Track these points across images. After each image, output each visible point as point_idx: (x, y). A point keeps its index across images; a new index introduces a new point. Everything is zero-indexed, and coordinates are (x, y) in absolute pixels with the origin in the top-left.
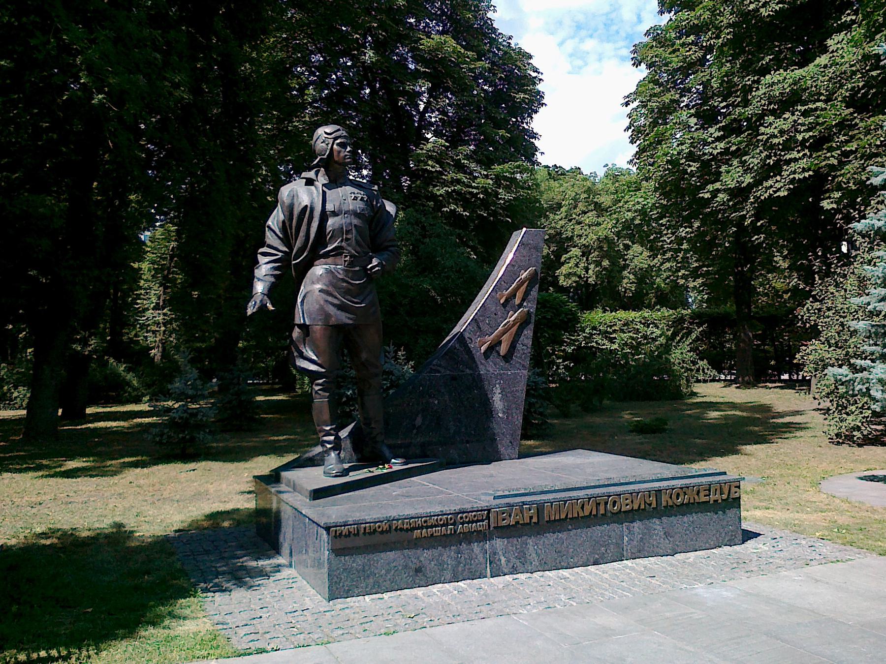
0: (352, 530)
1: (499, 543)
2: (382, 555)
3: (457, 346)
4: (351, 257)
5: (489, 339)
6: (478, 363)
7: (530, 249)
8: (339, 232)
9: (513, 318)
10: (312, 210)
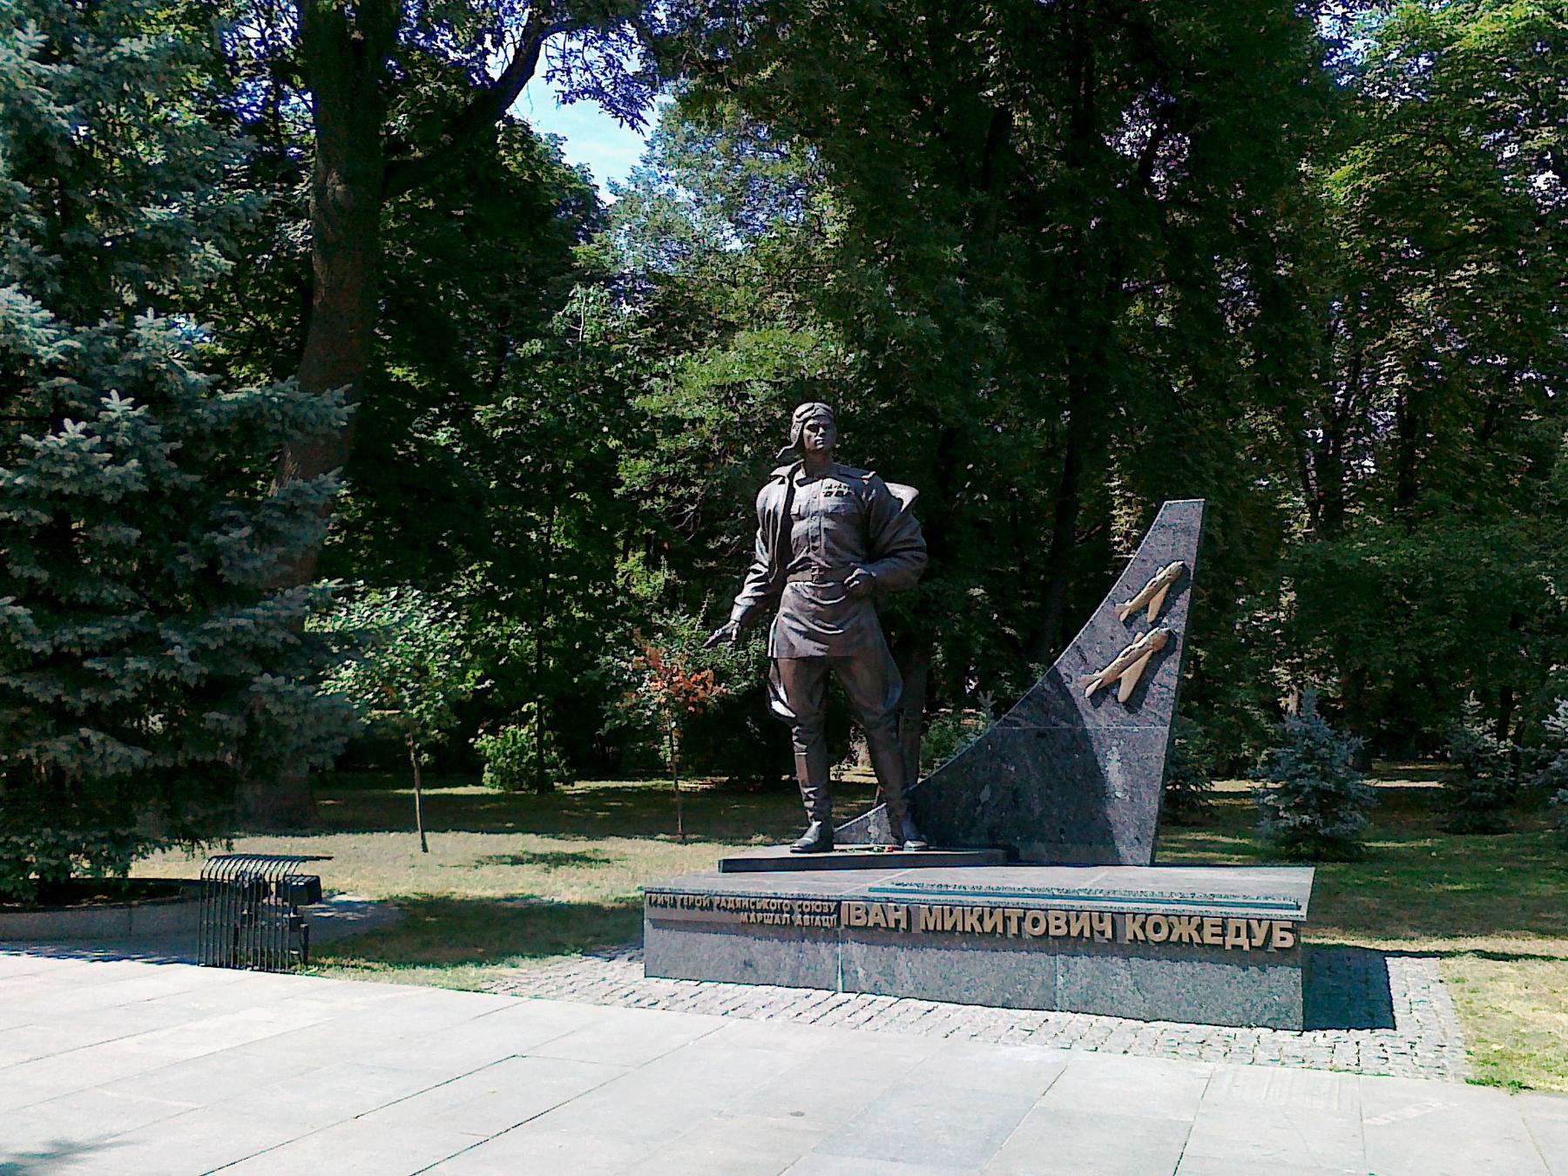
1: (855, 950)
3: (1047, 687)
10: (776, 515)
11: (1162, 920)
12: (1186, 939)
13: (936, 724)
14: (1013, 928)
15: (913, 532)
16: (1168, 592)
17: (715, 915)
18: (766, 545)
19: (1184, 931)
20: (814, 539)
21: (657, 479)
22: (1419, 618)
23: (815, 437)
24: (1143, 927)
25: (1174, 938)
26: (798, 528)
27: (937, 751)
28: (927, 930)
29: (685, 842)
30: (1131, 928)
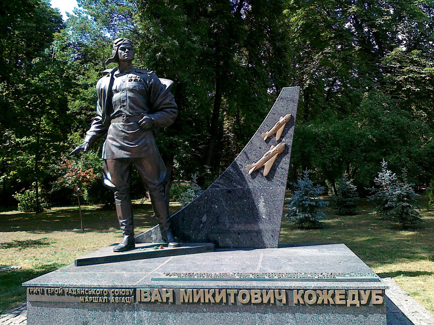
0: (39, 290)
1: (144, 314)
2: (61, 309)
5: (254, 166)
6: (248, 181)
10: (105, 91)
11: (313, 293)
12: (326, 302)
13: (173, 185)
14: (232, 300)
15: (171, 99)
16: (285, 127)
17: (66, 298)
18: (101, 107)
19: (325, 298)
20: (123, 102)
21: (82, 109)
22: (329, 148)
23: (123, 54)
24: (303, 297)
25: (319, 302)
26: (116, 96)
27: (174, 193)
28: (184, 303)
29: (84, 232)
30: (296, 298)
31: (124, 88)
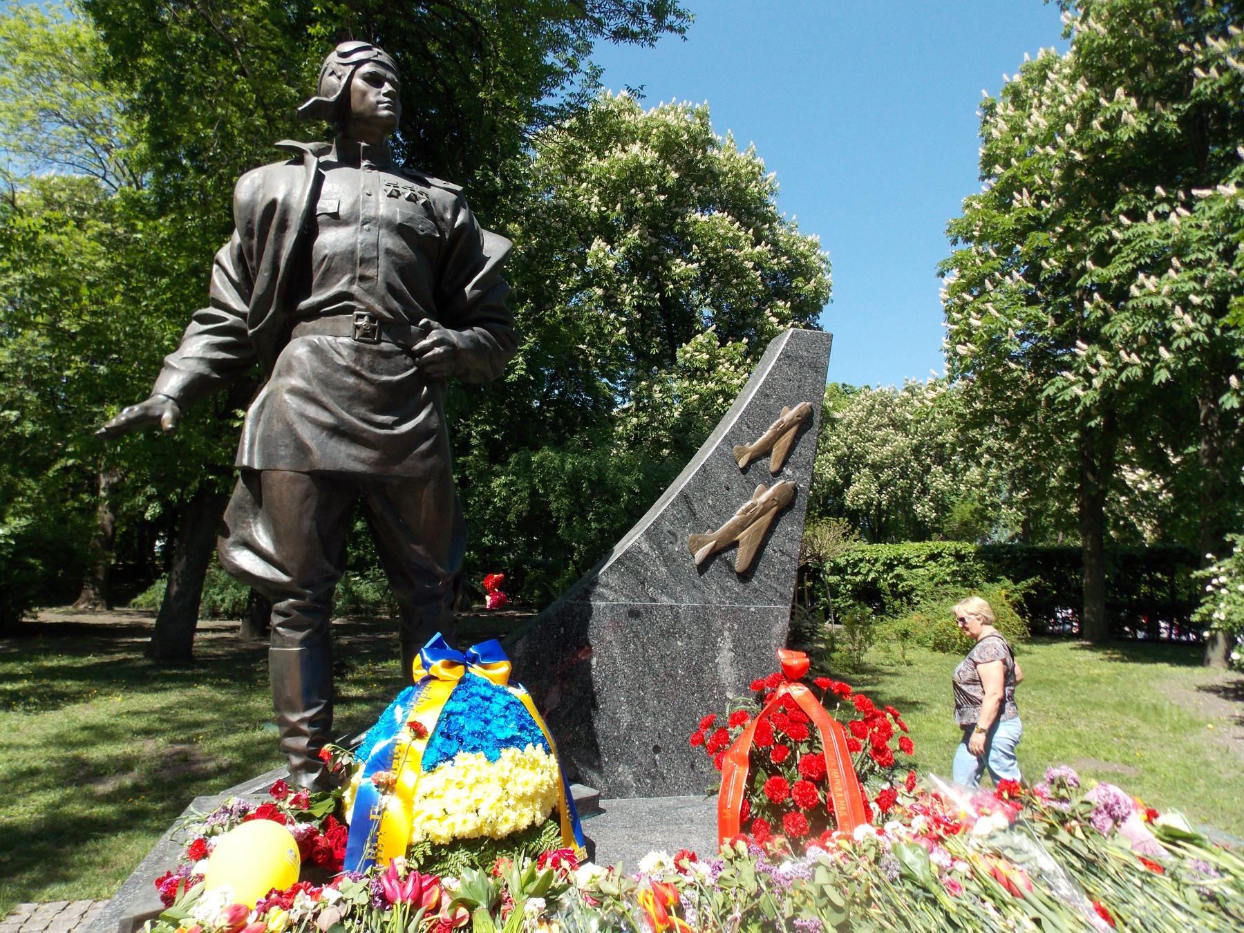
3: (645, 547)
4: (372, 319)
7: (801, 366)
8: (350, 259)
9: (763, 498)
20: (364, 261)
26: (330, 240)
31: (372, 214)
